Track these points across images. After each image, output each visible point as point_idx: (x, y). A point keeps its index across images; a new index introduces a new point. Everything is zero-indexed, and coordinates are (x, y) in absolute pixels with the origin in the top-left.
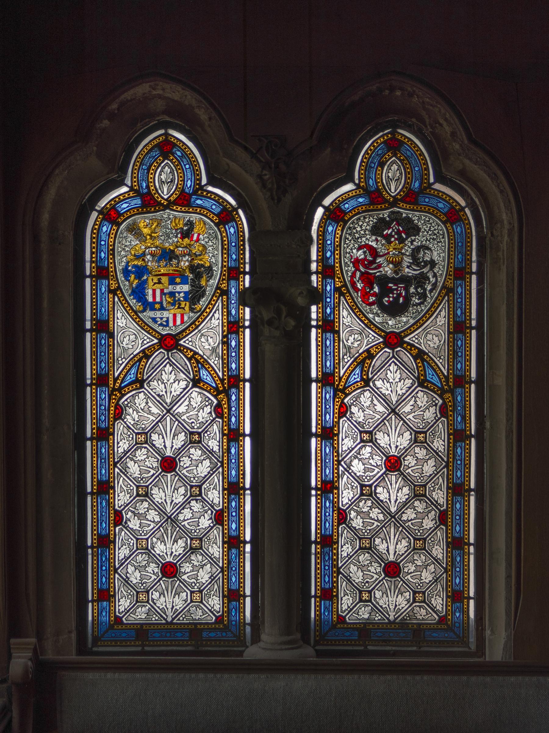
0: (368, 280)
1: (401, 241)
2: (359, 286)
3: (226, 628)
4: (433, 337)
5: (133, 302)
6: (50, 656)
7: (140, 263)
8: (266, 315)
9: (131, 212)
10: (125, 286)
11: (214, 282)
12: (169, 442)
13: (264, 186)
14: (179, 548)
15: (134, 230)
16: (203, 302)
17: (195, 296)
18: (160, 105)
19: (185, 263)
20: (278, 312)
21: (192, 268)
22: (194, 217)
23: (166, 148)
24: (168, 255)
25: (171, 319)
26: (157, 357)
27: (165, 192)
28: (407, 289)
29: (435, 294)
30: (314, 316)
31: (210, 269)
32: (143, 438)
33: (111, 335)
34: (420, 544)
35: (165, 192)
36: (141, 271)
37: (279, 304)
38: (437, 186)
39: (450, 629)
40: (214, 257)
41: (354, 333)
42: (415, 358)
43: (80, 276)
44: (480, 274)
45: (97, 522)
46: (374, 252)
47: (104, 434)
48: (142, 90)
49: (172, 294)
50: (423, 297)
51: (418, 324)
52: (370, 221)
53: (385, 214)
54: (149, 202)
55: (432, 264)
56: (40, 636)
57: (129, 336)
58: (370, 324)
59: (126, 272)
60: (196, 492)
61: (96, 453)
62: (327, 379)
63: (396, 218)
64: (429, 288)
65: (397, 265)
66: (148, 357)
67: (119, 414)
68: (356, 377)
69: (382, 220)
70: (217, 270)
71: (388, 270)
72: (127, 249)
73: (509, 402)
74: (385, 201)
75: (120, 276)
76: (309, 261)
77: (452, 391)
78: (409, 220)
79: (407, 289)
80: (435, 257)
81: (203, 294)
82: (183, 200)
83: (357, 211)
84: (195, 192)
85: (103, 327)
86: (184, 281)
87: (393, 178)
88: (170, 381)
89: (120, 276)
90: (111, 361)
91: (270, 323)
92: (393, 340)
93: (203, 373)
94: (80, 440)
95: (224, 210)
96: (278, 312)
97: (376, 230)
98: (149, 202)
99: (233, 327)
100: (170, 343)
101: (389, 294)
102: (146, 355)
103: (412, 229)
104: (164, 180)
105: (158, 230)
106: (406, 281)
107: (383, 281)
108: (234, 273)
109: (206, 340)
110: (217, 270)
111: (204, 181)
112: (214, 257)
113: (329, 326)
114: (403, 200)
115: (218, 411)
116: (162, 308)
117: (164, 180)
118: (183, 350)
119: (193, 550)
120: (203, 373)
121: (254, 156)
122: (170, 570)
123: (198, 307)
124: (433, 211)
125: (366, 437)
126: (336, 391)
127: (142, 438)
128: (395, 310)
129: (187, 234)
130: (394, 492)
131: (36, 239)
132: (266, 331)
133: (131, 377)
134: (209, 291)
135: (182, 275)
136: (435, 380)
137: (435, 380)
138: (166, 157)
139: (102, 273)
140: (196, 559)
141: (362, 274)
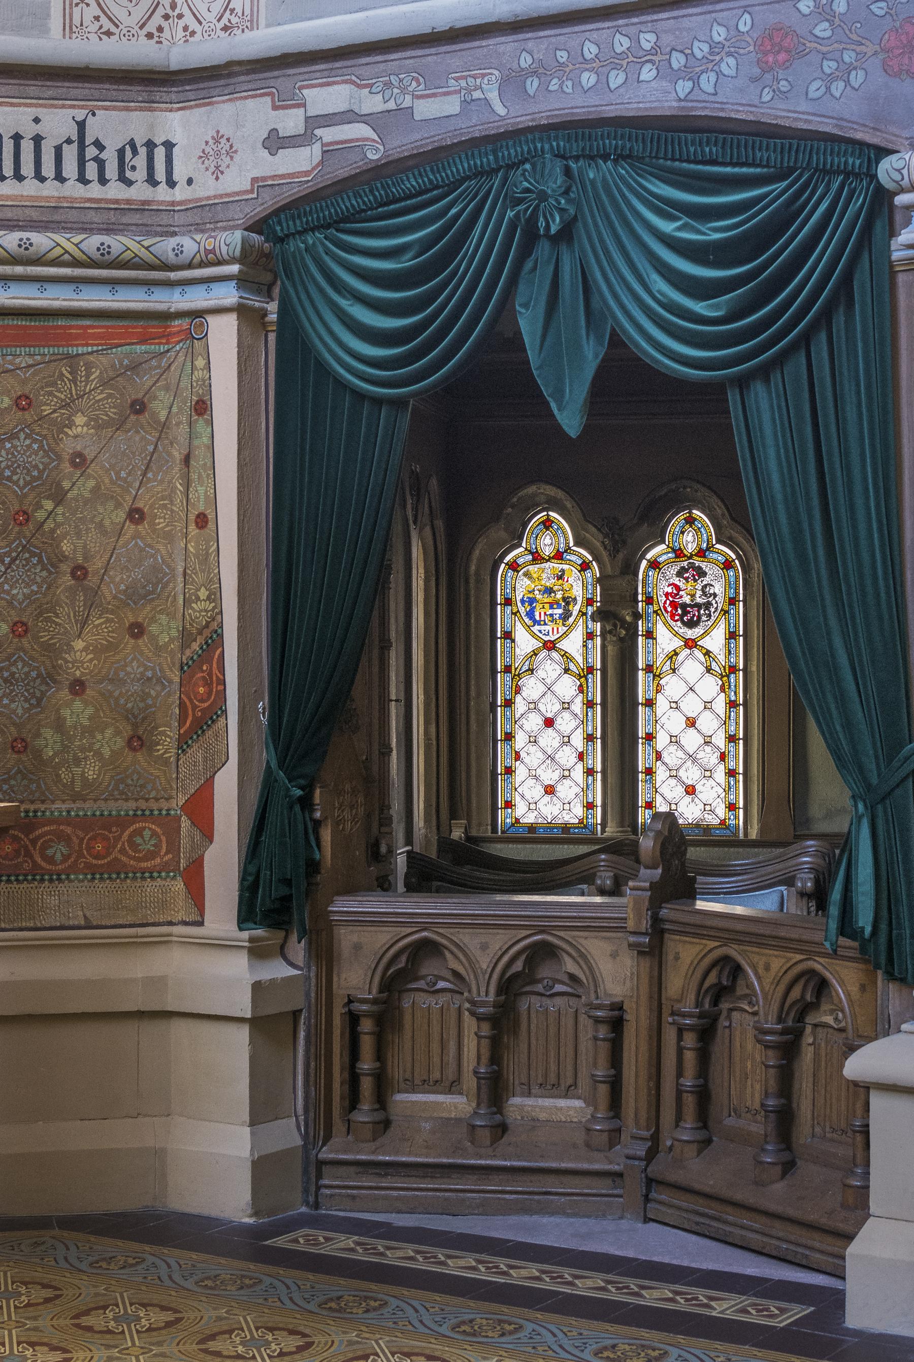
0: (674, 605)
1: (695, 581)
2: (669, 609)
3: (585, 827)
4: (716, 641)
5: (527, 620)
6: (474, 833)
7: (531, 596)
8: (608, 628)
9: (526, 564)
10: (522, 610)
11: (577, 607)
12: (550, 707)
13: (605, 548)
14: (556, 775)
15: (527, 575)
16: (571, 620)
17: (566, 616)
18: (543, 498)
19: (559, 595)
20: (615, 626)
21: (564, 599)
22: (566, 567)
23: (547, 524)
24: (549, 591)
25: (550, 631)
26: (543, 654)
27: (548, 551)
28: (699, 611)
29: (717, 614)
30: (640, 628)
31: (575, 599)
32: (534, 706)
33: (513, 641)
34: (708, 773)
35: (548, 551)
36: (532, 601)
37: (619, 619)
38: (718, 546)
39: (728, 828)
40: (577, 591)
41: (666, 639)
42: (705, 655)
43: (493, 604)
44: (745, 601)
45: (504, 758)
46: (678, 588)
47: (509, 703)
48: (531, 489)
49: (551, 615)
50: (709, 616)
51: (706, 633)
52: (675, 569)
53: (686, 563)
54: (537, 558)
55: (715, 595)
56: (469, 818)
57: (525, 642)
58: (676, 634)
59: (523, 602)
60: (566, 741)
61: (504, 715)
62: (649, 669)
63: (692, 566)
64: (713, 610)
65: (693, 596)
66: (536, 655)
67: (518, 690)
68: (667, 667)
69: (683, 568)
70: (579, 600)
71: (687, 599)
72: (523, 586)
73: (758, 681)
74: (685, 556)
75: (519, 604)
76: (636, 594)
77: (728, 676)
78: (700, 568)
79: (699, 611)
80: (717, 591)
81: (571, 615)
82: (559, 556)
83: (669, 563)
84: (566, 551)
85: (508, 635)
86: (559, 606)
87: (689, 542)
88: (549, 668)
89: (519, 604)
90: (513, 655)
91: (610, 632)
92: (690, 644)
93: (571, 665)
94: (493, 706)
95: (584, 562)
96: (615, 626)
97: (680, 574)
98: (537, 558)
99: (590, 636)
100: (550, 646)
101: (688, 615)
102: (535, 653)
103: (702, 573)
104: (547, 544)
105: (546, 572)
106: (698, 606)
107: (684, 606)
108: (590, 602)
109: (573, 644)
110: (579, 600)
111: (571, 544)
112: (577, 591)
113: (650, 635)
114: (696, 555)
115: (581, 689)
116: (545, 624)
117: (547, 544)
118: (558, 650)
119: (564, 777)
120: (571, 665)
121: (599, 530)
122: (550, 790)
123: (567, 623)
124: (715, 562)
125: (674, 705)
126: (654, 676)
127: (532, 706)
128: (691, 624)
129: (560, 577)
130: (692, 740)
131: (467, 582)
132: (608, 636)
133: (526, 667)
134: (575, 613)
135: (557, 603)
136: (717, 669)
137: (717, 669)
138: (547, 529)
139: (508, 602)
140: (567, 782)
141: (671, 602)
